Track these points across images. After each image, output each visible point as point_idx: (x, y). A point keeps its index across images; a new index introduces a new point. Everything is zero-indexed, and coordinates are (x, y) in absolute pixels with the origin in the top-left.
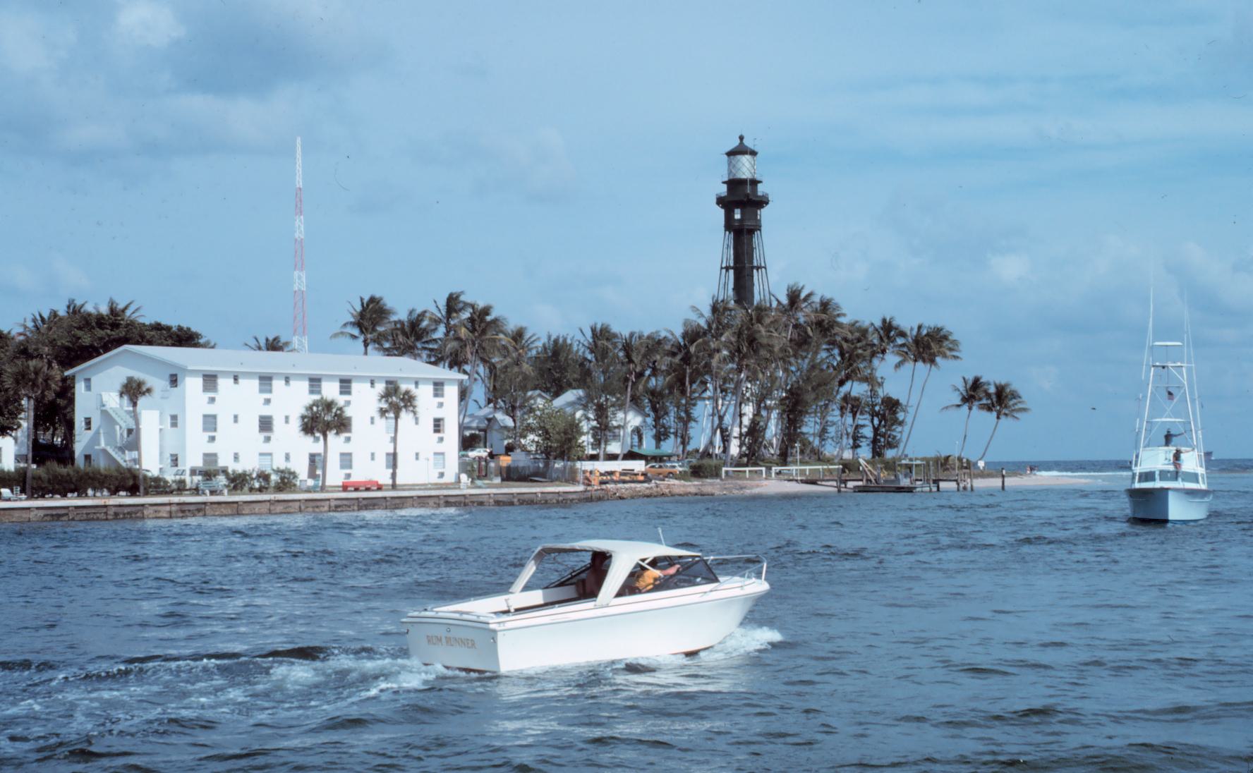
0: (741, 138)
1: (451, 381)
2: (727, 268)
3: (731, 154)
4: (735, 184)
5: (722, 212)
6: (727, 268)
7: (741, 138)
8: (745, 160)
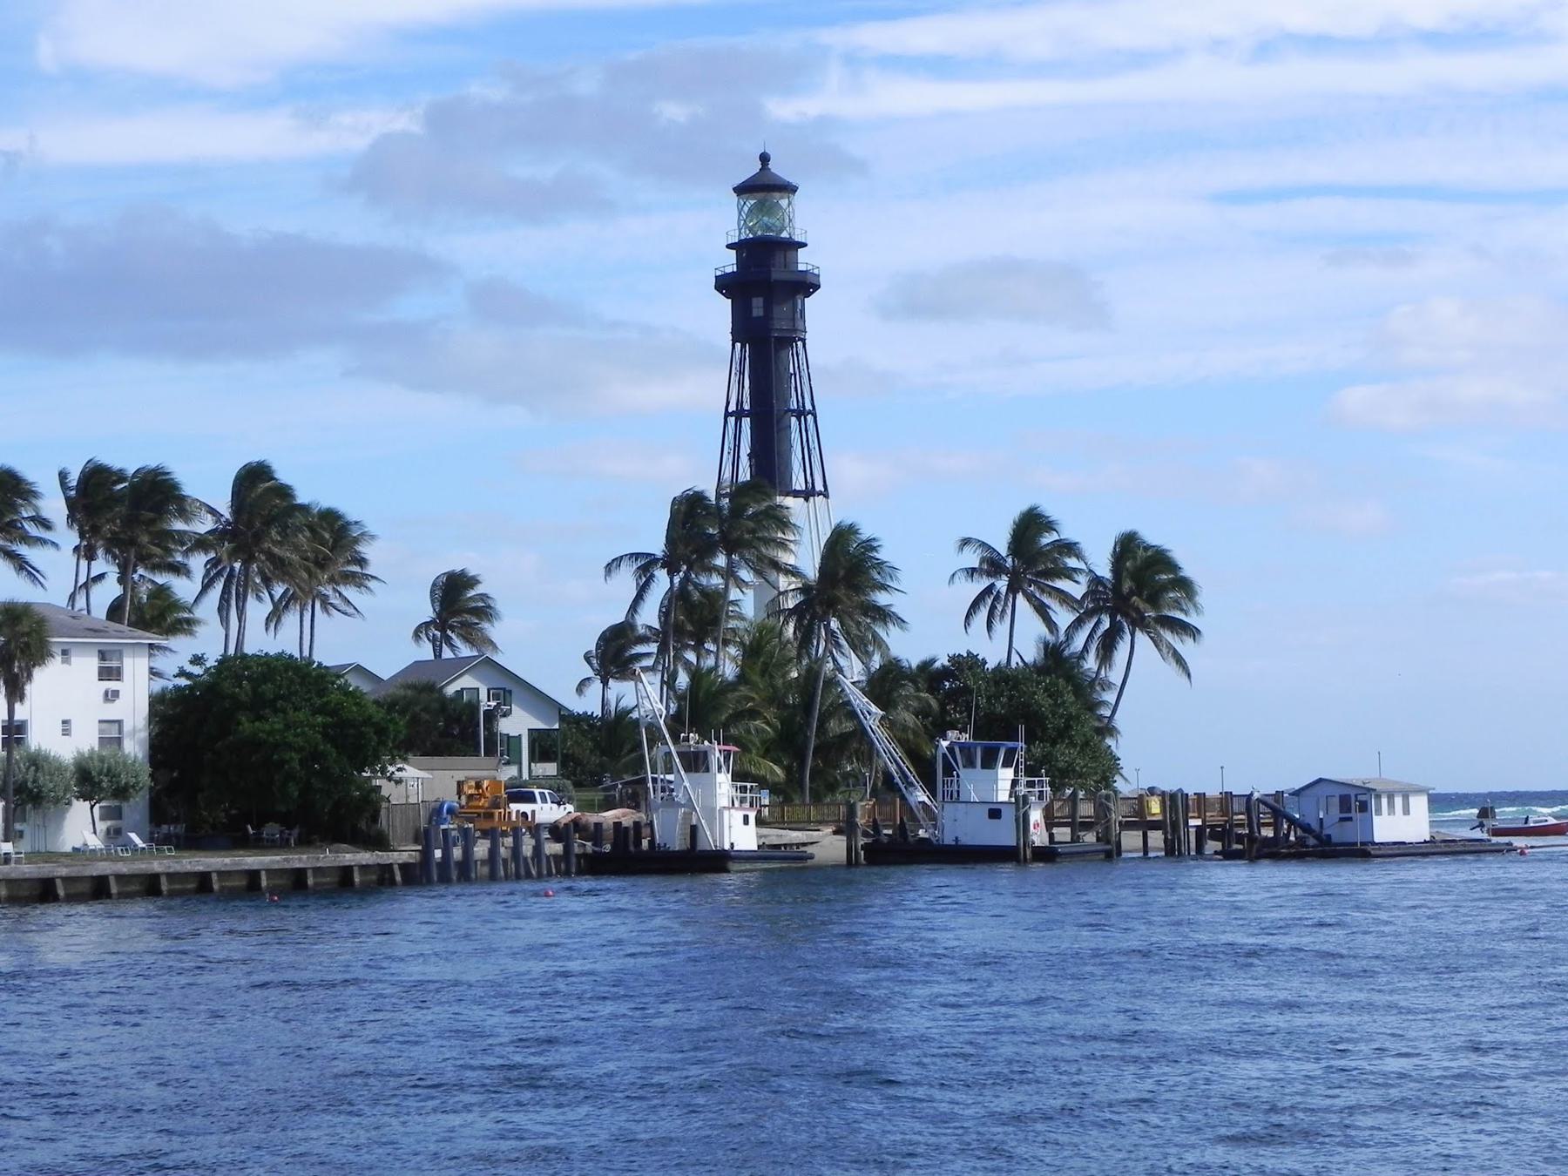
0: (765, 158)
5: (727, 304)
6: (739, 414)
7: (765, 158)
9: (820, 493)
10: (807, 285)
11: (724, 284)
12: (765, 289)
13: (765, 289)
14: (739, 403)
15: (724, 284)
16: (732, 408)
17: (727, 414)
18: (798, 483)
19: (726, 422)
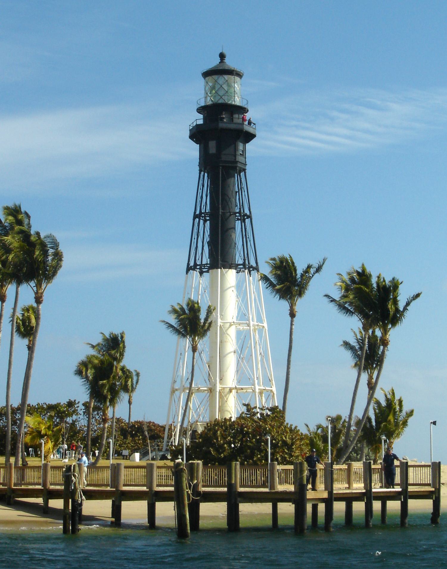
0: (222, 56)
5: (197, 146)
7: (222, 56)
11: (197, 134)
12: (221, 136)
13: (221, 136)
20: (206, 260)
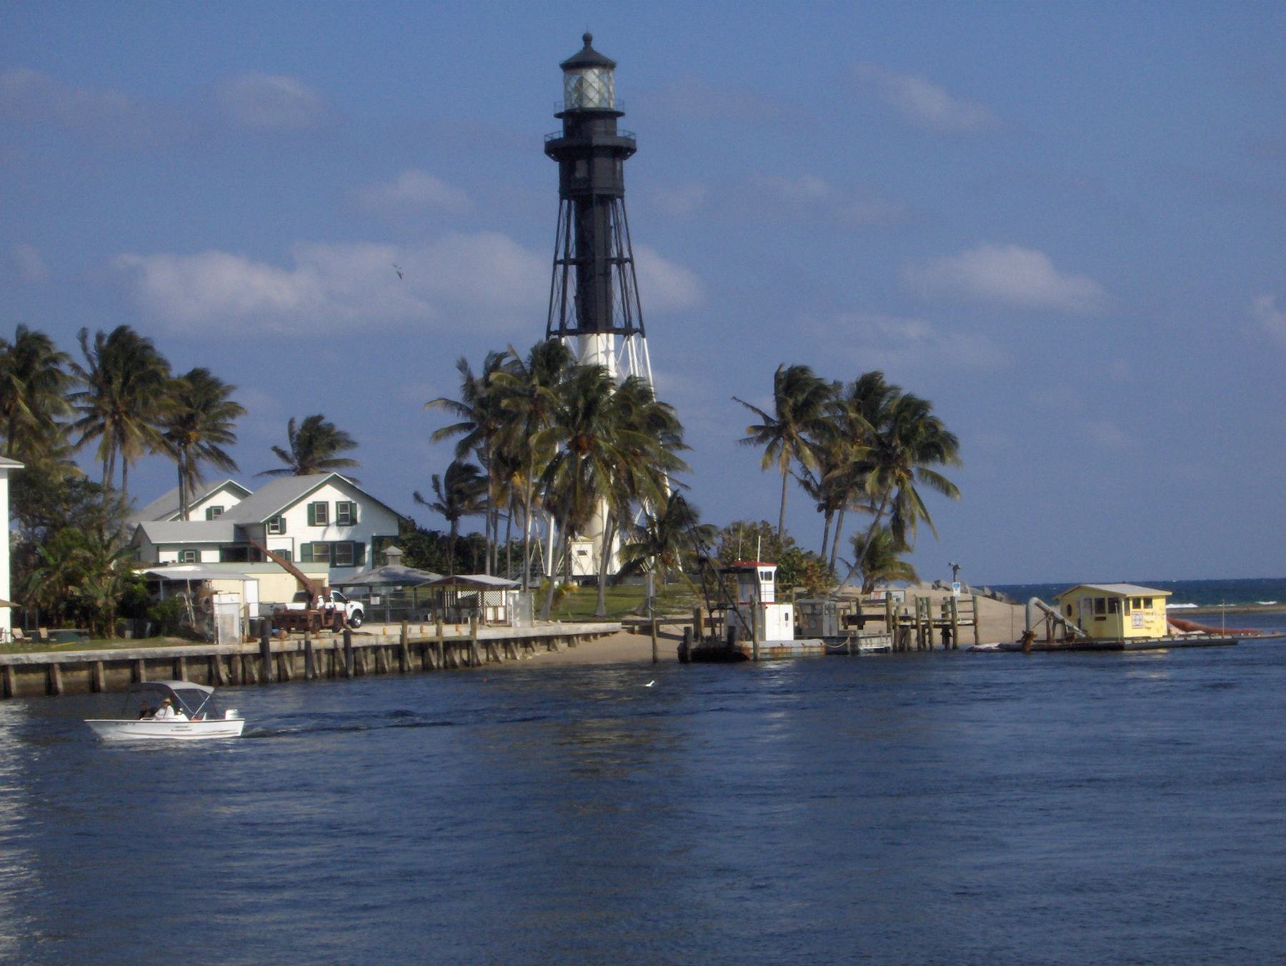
0: (587, 39)
1: (1158, 597)
2: (566, 262)
3: (574, 66)
4: (579, 120)
6: (566, 262)
7: (587, 39)
8: (592, 76)
9: (636, 331)
10: (623, 151)
11: (553, 149)
12: (587, 154)
13: (587, 154)
14: (567, 254)
15: (553, 149)
16: (561, 256)
17: (556, 262)
18: (618, 321)
19: (555, 269)
20: (572, 324)
